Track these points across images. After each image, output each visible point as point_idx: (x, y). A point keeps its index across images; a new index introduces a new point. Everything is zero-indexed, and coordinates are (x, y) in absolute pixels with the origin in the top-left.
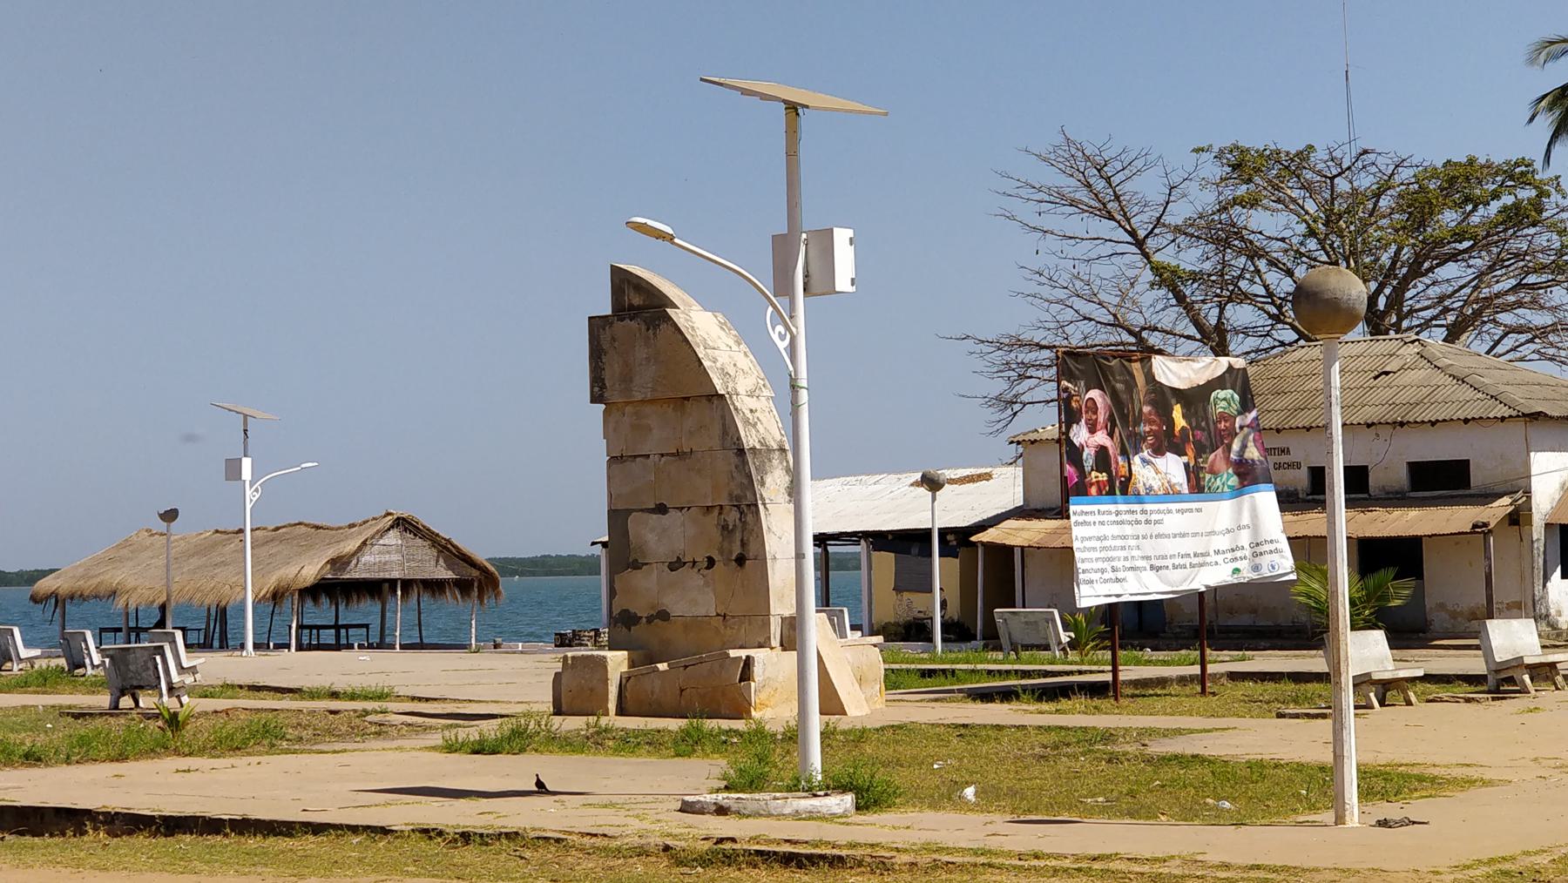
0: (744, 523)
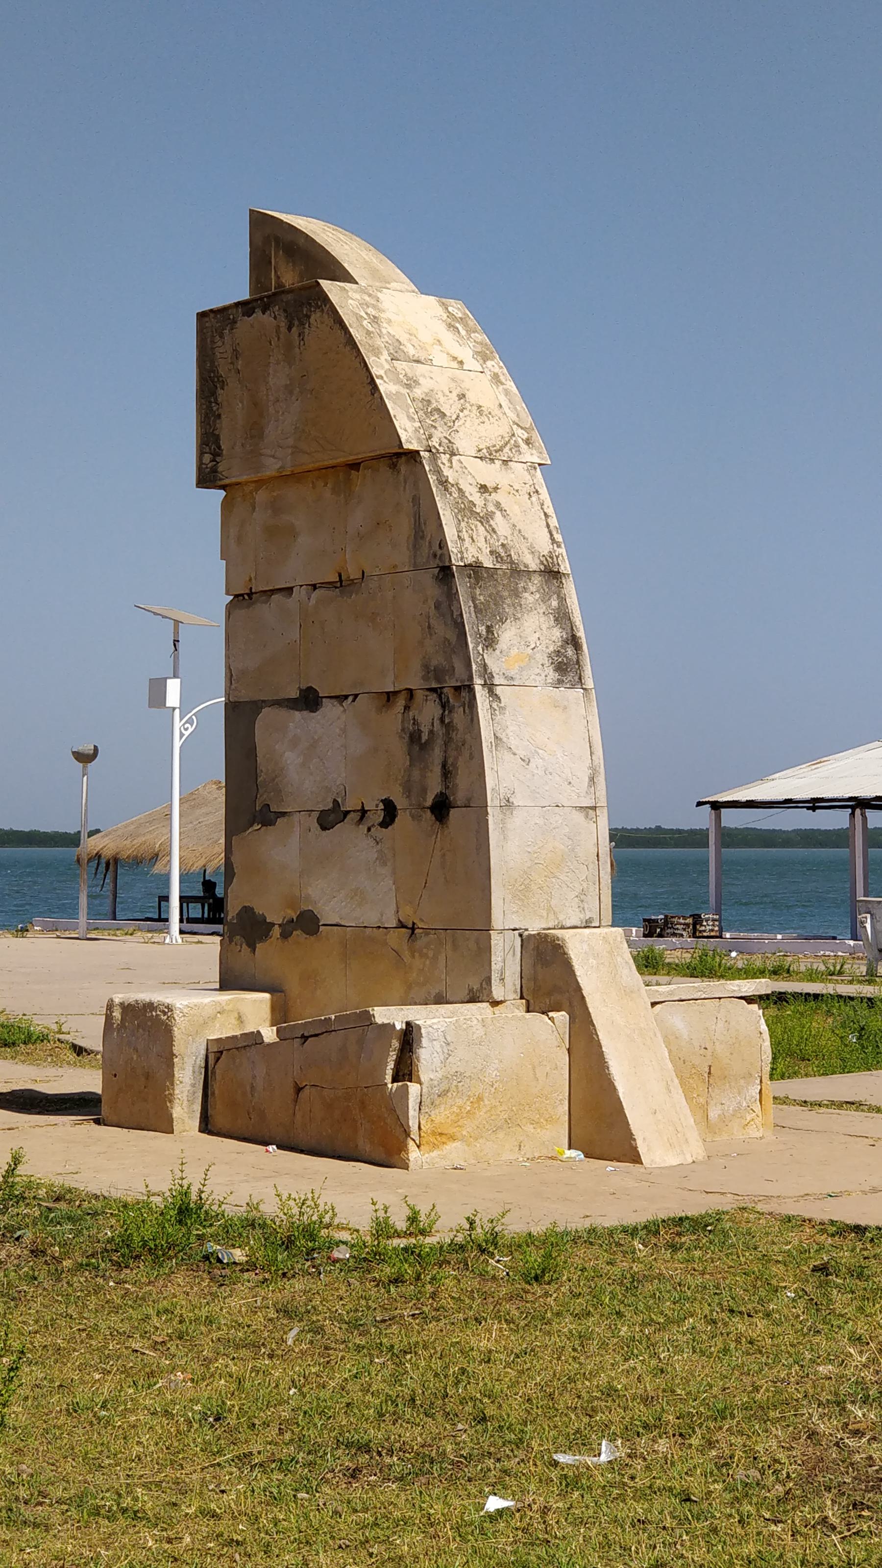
0: (448, 727)
